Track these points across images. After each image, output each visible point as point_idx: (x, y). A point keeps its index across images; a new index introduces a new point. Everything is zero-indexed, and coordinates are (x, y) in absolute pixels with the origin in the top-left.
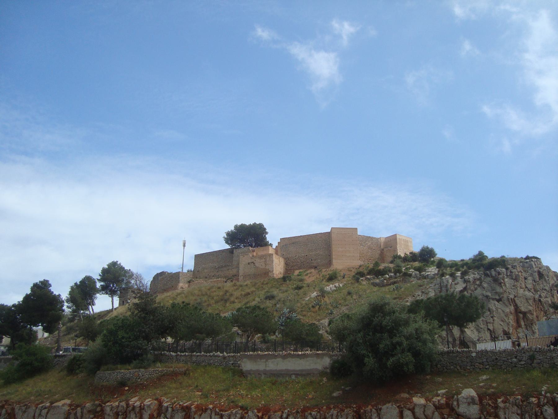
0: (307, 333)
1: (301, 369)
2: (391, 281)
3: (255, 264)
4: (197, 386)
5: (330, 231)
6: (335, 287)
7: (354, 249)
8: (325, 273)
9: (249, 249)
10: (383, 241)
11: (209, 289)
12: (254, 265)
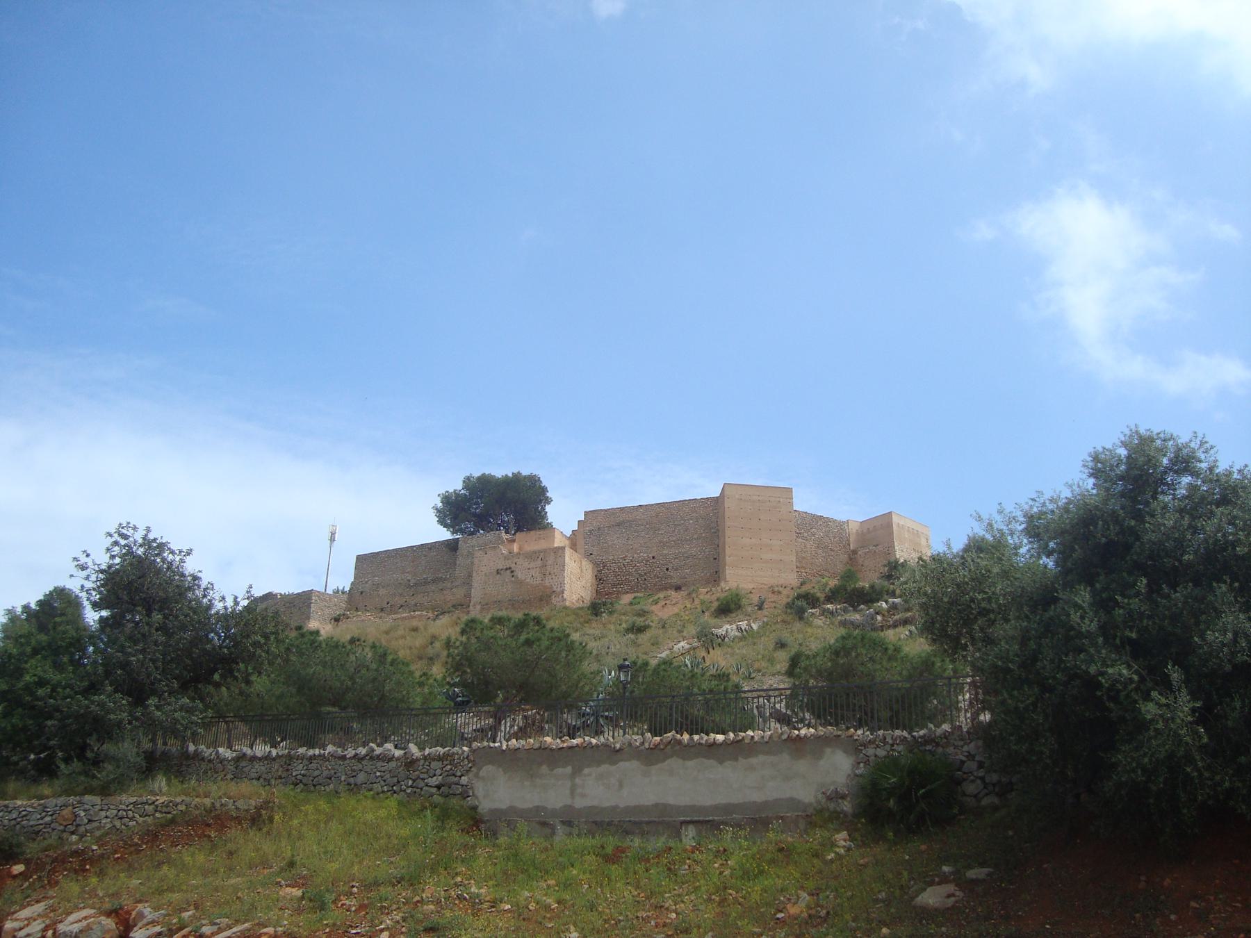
0: (707, 702)
1: (724, 801)
2: (897, 617)
4: (291, 864)
6: (739, 629)
7: (782, 543)
8: (708, 597)
9: (500, 537)
10: (854, 531)
11: (387, 633)
12: (513, 576)
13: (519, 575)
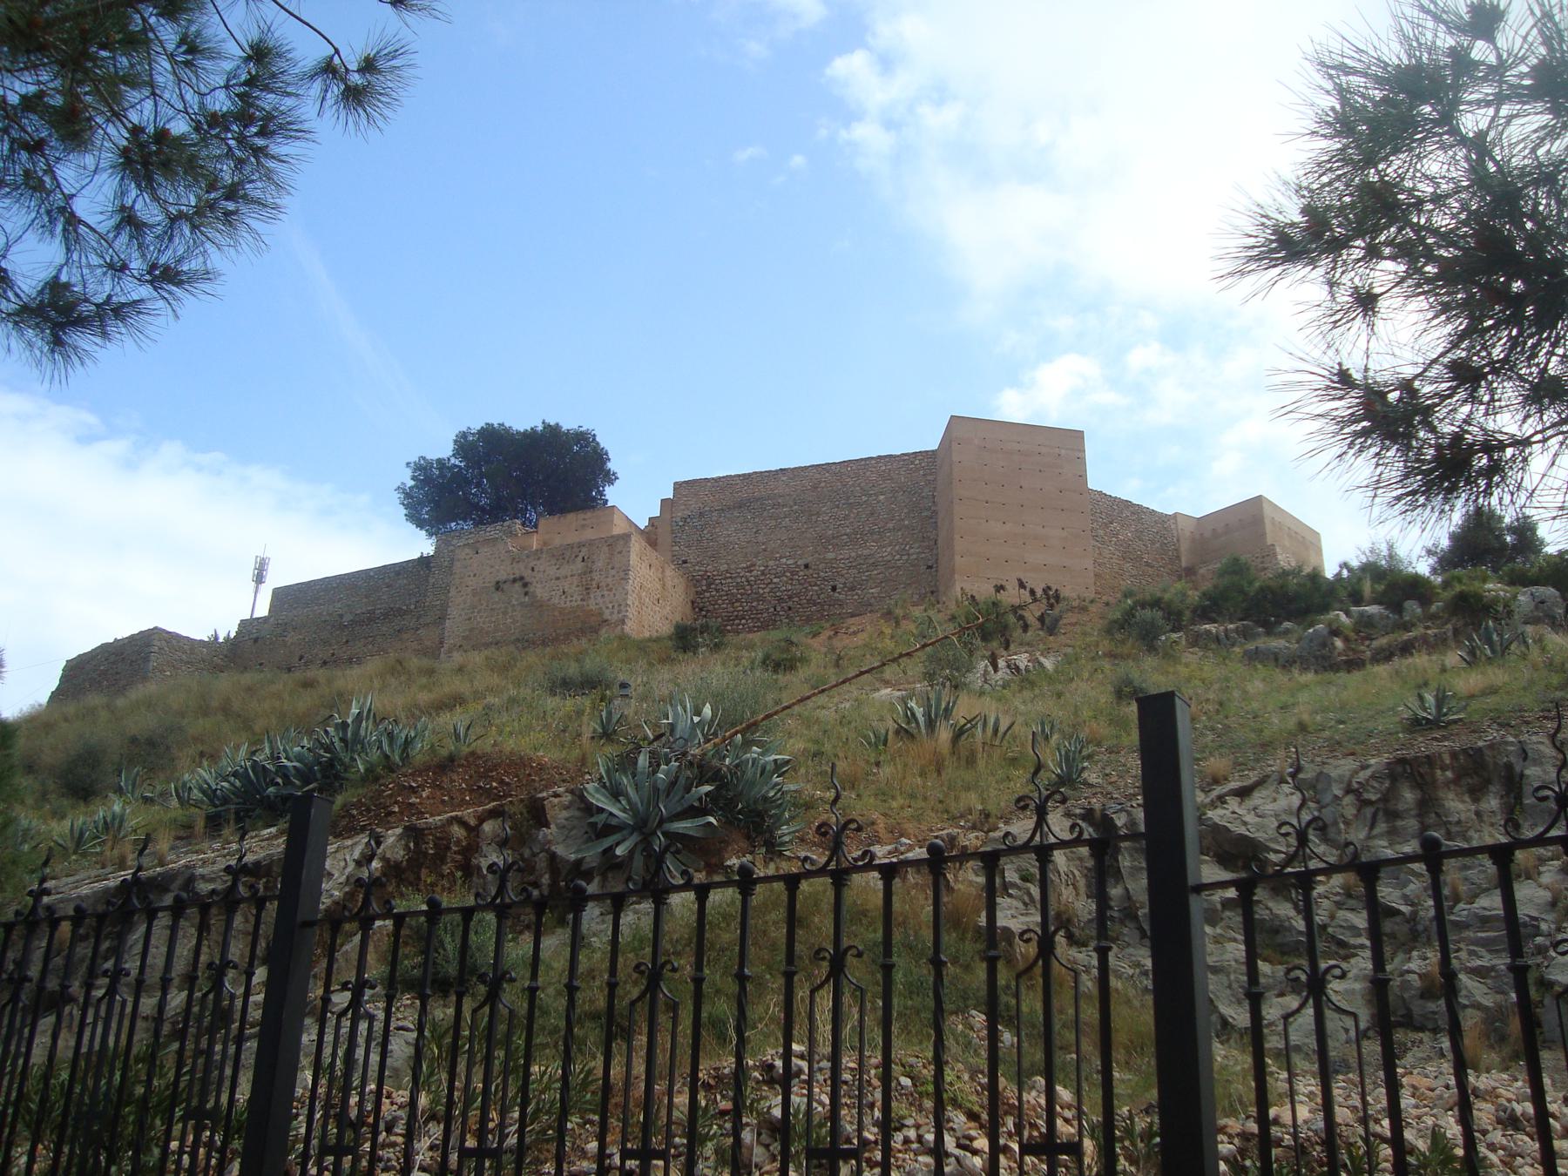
5: (932, 443)
10: (1188, 534)
12: (526, 594)
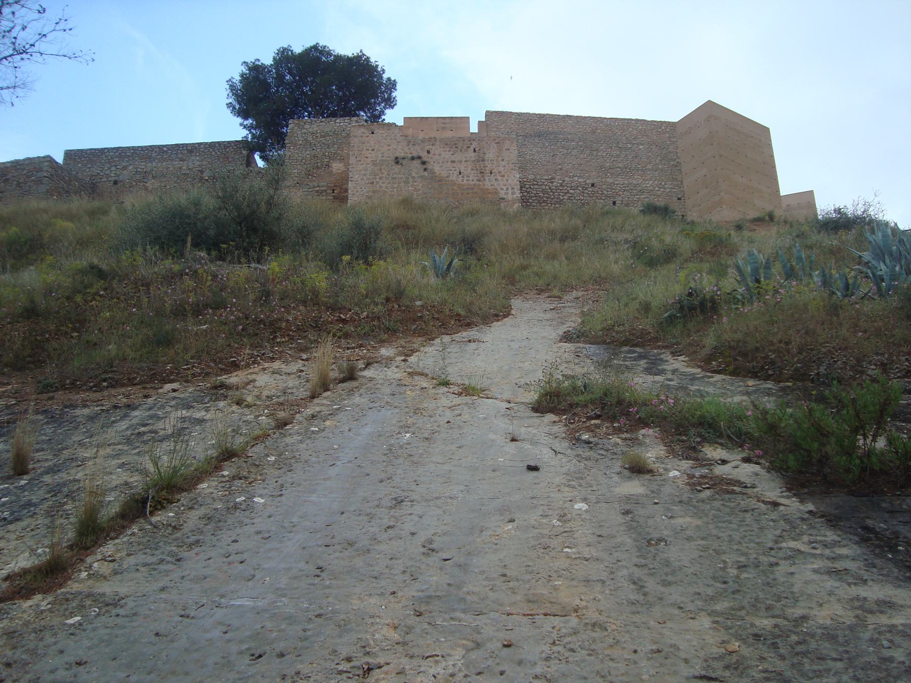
3: (429, 167)
13: (437, 169)
